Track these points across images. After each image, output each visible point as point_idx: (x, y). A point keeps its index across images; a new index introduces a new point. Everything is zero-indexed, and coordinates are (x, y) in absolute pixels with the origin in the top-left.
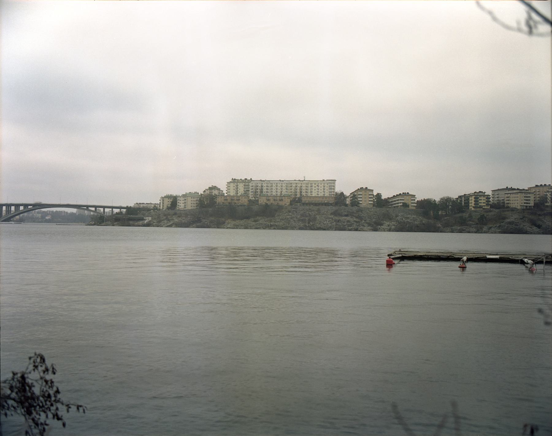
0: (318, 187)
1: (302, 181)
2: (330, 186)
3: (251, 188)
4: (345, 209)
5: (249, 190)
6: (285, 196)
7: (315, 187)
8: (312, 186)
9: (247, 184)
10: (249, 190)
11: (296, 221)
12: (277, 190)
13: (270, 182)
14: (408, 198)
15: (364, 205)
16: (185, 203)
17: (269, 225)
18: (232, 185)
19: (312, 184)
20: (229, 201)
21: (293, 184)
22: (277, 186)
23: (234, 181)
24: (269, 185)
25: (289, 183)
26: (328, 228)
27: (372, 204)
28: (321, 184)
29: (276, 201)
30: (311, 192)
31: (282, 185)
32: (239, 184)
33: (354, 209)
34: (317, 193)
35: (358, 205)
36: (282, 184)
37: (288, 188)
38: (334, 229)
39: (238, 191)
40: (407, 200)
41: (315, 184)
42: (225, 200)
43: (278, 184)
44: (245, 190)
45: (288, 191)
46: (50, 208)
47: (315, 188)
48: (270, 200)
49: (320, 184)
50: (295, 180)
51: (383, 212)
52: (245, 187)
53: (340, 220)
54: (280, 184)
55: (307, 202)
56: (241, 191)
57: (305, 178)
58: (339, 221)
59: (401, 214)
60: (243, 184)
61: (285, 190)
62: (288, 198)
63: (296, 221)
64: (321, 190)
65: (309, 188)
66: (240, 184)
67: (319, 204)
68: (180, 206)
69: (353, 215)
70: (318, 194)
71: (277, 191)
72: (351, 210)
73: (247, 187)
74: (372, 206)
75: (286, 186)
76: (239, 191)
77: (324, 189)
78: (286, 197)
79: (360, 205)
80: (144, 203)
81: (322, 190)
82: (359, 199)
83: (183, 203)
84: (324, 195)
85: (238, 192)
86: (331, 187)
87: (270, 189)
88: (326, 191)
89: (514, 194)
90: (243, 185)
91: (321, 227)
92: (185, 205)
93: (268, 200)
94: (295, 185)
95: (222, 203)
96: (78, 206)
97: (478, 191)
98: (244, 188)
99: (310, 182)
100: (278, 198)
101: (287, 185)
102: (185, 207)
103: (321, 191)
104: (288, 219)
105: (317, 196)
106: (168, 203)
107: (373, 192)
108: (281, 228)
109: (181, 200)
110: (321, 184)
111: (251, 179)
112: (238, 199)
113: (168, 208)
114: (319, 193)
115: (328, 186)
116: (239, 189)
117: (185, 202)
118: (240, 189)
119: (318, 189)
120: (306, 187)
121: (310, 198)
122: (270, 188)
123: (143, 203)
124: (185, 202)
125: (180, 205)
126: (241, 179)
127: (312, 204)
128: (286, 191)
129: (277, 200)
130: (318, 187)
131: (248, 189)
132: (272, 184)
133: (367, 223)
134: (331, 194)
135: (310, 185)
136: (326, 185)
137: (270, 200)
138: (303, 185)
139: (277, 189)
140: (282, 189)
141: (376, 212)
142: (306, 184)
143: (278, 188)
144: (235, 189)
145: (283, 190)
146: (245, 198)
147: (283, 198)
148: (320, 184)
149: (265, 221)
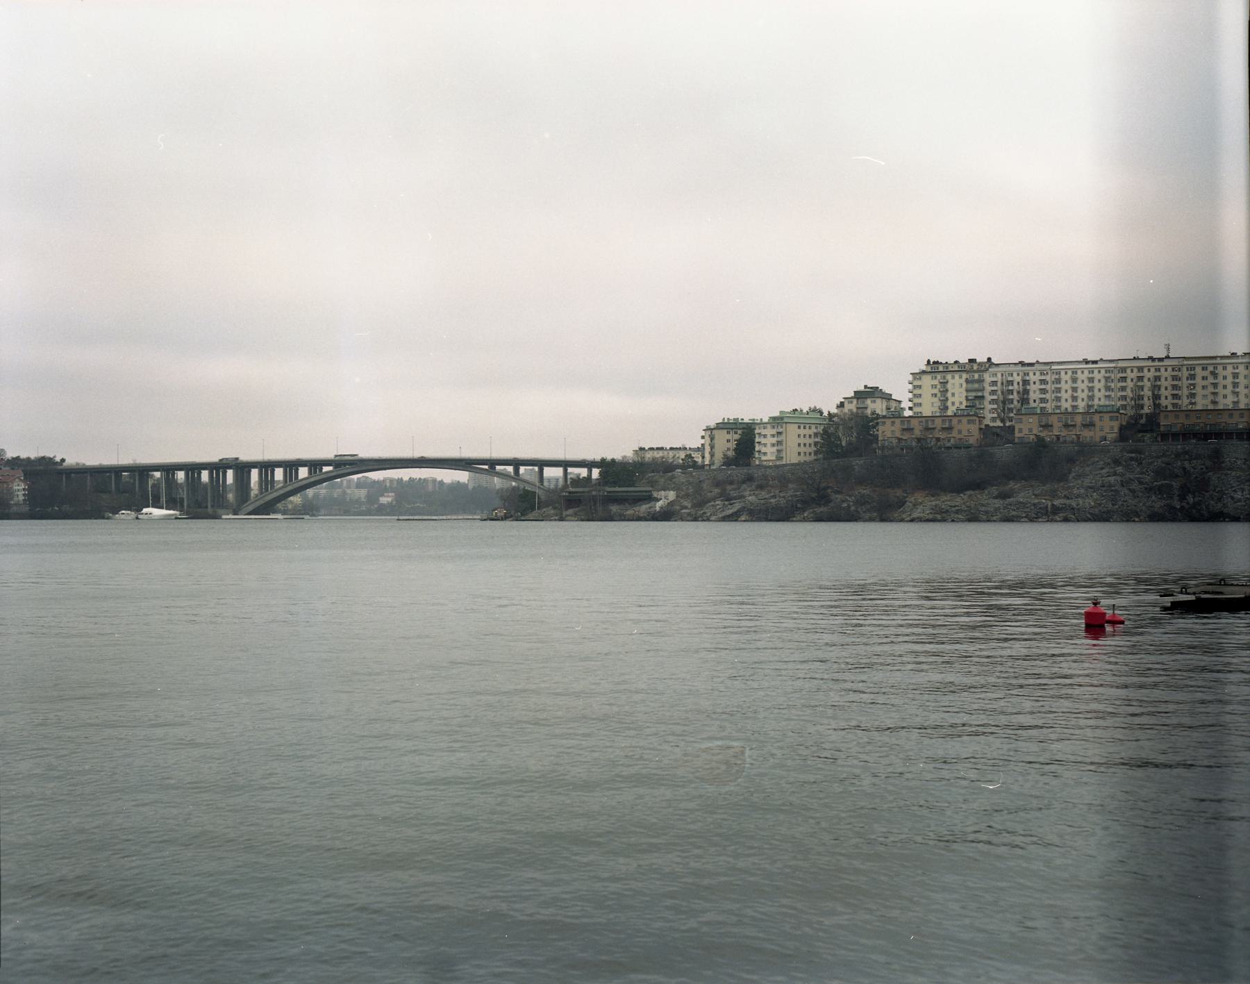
3: (989, 388)
7: (1204, 378)
8: (1192, 377)
9: (976, 376)
13: (1053, 367)
16: (779, 443)
17: (1047, 507)
18: (927, 381)
19: (1192, 368)
21: (1129, 371)
22: (1074, 380)
23: (934, 367)
24: (1048, 378)
28: (1225, 368)
30: (1193, 395)
31: (1091, 376)
32: (949, 377)
34: (1211, 397)
37: (1113, 385)
39: (947, 399)
41: (1203, 369)
42: (904, 430)
44: (970, 398)
47: (1205, 383)
48: (1094, 425)
52: (970, 386)
54: (1086, 372)
56: (957, 399)
60: (965, 376)
61: (1103, 390)
63: (1140, 494)
68: (765, 454)
70: (1214, 402)
71: (1075, 394)
73: (976, 386)
75: (1107, 379)
78: (1106, 417)
81: (1230, 388)
90: (963, 381)
91: (1225, 511)
98: (967, 391)
100: (1079, 420)
101: (1107, 375)
102: (779, 458)
104: (1110, 486)
105: (1210, 407)
113: (728, 462)
116: (949, 395)
117: (778, 442)
118: (953, 395)
122: (1053, 386)
123: (660, 446)
124: (778, 442)
126: (956, 362)
127: (1195, 435)
128: (1107, 394)
131: (980, 394)
137: (1052, 426)
138: (1096, 375)
140: (1091, 389)
142: (1173, 370)
144: (939, 395)
145: (1096, 391)
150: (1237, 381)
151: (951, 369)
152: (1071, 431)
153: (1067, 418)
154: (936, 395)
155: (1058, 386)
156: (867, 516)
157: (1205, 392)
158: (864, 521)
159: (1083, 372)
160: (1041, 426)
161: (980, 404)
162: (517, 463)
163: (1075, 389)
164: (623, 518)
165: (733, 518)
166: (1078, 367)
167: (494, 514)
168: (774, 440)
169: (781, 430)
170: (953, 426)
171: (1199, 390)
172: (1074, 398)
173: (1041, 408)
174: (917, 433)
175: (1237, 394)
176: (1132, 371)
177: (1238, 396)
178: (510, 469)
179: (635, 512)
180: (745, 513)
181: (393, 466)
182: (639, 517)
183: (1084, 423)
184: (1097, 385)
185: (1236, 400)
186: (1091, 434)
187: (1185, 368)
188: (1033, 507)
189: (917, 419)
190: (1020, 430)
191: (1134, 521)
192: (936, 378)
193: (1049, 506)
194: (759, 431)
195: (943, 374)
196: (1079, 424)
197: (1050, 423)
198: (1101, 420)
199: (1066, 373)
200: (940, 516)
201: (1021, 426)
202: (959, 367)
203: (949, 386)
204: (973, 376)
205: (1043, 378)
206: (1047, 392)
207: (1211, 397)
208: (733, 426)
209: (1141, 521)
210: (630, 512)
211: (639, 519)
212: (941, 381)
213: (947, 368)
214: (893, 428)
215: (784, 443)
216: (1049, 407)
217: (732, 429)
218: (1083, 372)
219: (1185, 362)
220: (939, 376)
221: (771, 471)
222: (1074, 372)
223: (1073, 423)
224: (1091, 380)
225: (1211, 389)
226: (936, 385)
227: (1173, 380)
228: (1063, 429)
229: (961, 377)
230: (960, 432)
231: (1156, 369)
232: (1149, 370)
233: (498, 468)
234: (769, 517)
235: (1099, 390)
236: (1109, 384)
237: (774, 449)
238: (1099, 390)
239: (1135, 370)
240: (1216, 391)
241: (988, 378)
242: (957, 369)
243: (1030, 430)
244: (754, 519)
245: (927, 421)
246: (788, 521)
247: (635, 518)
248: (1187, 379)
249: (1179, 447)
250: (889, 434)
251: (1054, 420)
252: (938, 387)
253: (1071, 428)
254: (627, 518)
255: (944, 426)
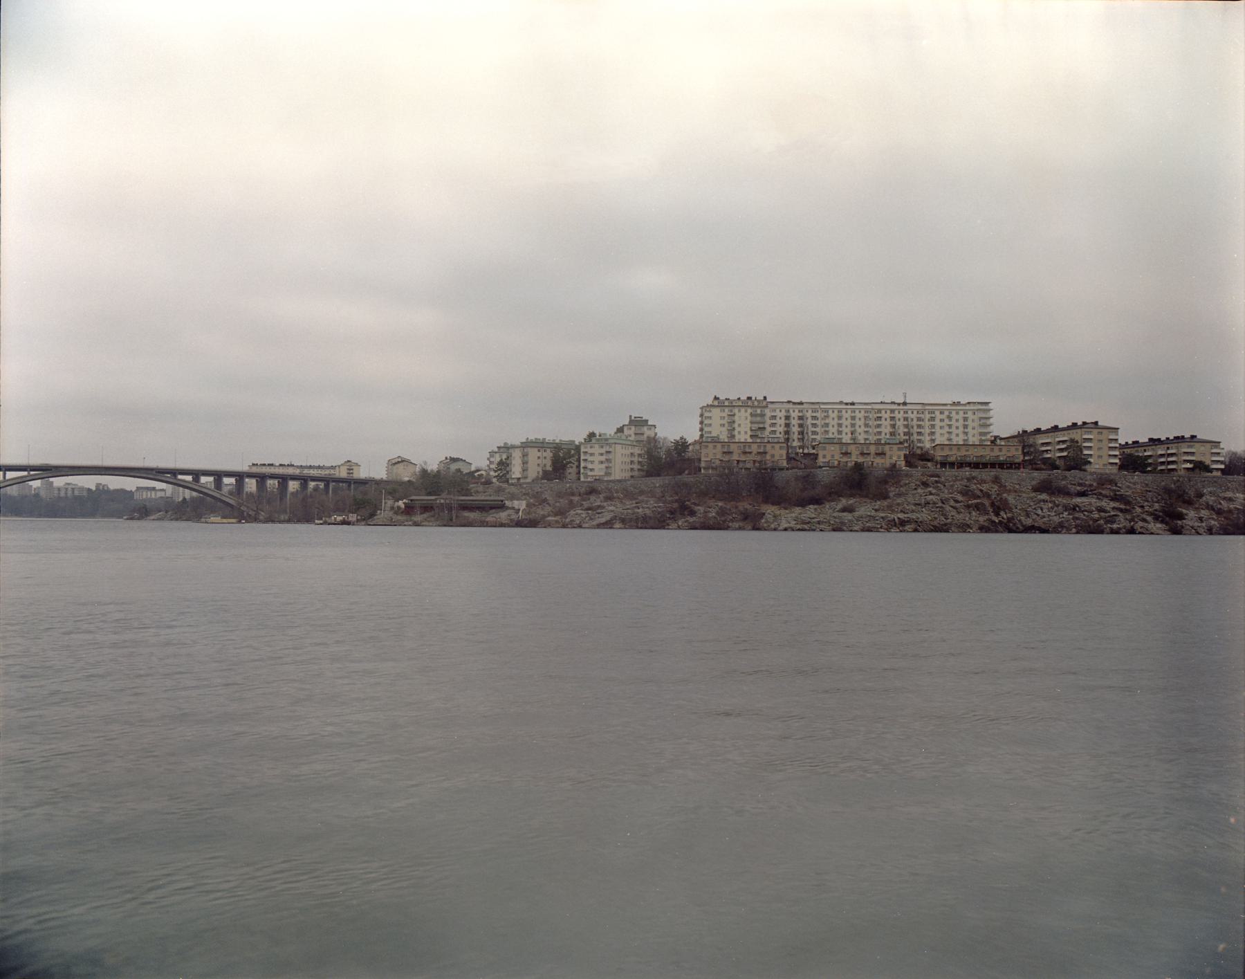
0: (950, 420)
1: (899, 404)
2: (981, 419)
3: (769, 422)
4: (1066, 477)
5: (764, 428)
6: (889, 444)
7: (942, 420)
8: (933, 419)
9: (759, 411)
10: (764, 428)
11: (963, 510)
12: (841, 427)
13: (822, 407)
14: (1203, 448)
15: (1097, 467)
16: (608, 460)
17: (894, 520)
18: (716, 413)
19: (933, 412)
20: (855, 458)
21: (883, 412)
22: (840, 418)
23: (718, 403)
24: (818, 415)
25: (874, 413)
26: (1054, 528)
27: (1116, 464)
28: (957, 413)
29: (748, 455)
30: (932, 433)
31: (853, 414)
32: (736, 410)
33: (1088, 477)
34: (947, 436)
35: (1083, 467)
36: (855, 412)
37: (870, 423)
38: (1074, 530)
39: (734, 429)
40: (1201, 454)
41: (941, 413)
42: (724, 453)
43: (844, 411)
44: (753, 428)
45: (870, 430)
46: (68, 475)
47: (942, 424)
48: (885, 454)
49: (954, 413)
50: (882, 403)
51: (1163, 483)
52: (755, 419)
53: (1078, 506)
54: (849, 411)
55: (952, 459)
56: (742, 430)
57: (905, 397)
58: (1074, 509)
59: (1209, 489)
60: (749, 410)
61: (863, 427)
62: (899, 449)
63: (963, 510)
64: (957, 428)
65: (927, 423)
66: (739, 411)
67: (983, 464)
68: (592, 470)
69: (1101, 494)
70: (950, 440)
71: (840, 429)
72: (1082, 480)
73: (758, 419)
74: (1115, 469)
75: (866, 418)
76: (737, 429)
77: (965, 427)
78: (895, 447)
79: (1087, 467)
80: (272, 465)
81: (961, 429)
82: (1086, 452)
83: (602, 462)
84: (964, 440)
85: (736, 433)
86: (983, 421)
87: (823, 426)
88: (969, 430)
89: (957, 441)
90: (748, 414)
91: (1036, 524)
92: (607, 467)
93: (846, 454)
94: (888, 415)
95: (718, 462)
96: (154, 472)
97: (1143, 439)
98: (751, 423)
99: (927, 407)
100: (873, 449)
101: (866, 415)
102: (608, 474)
103: (957, 431)
104: (934, 503)
105: (947, 443)
106: (538, 462)
107: (1117, 435)
108: (932, 528)
109: (592, 454)
110: (957, 413)
111: (765, 398)
112: (761, 450)
113: (546, 475)
114: (953, 437)
115: (975, 417)
116: (736, 425)
117: (607, 460)
118: (739, 425)
119: (950, 426)
120: (919, 419)
121: (958, 448)
122: (823, 422)
123: (271, 463)
124: (607, 460)
125: (590, 466)
126: (739, 399)
127: (969, 464)
128: (866, 429)
129: (869, 454)
130: (950, 420)
131: (761, 426)
132: (826, 411)
133: (1150, 514)
134: (983, 438)
135: (928, 416)
136: (970, 415)
137: (850, 453)
138: (857, 414)
139: (840, 425)
140: (853, 425)
141: (1147, 485)
142: (918, 412)
143: (843, 421)
144: (726, 425)
145: (857, 427)
146: (781, 448)
147: (887, 448)
148: (954, 413)
149: (876, 510)
150: (966, 423)
151: (734, 404)
152: (866, 458)
153: (863, 448)
154: (724, 425)
155: (933, 423)
156: (737, 525)
157: (942, 431)
158: (733, 530)
159: (860, 412)
160: (842, 453)
161: (761, 434)
162: (197, 474)
163: (840, 425)
164: (484, 524)
165: (608, 525)
166: (835, 407)
167: (333, 518)
168: (603, 458)
169: (611, 450)
170: (767, 451)
171: (937, 430)
172: (840, 432)
173: (839, 439)
174: (854, 458)
175: (966, 433)
176: (886, 412)
177: (967, 435)
178: (189, 478)
179: (497, 519)
180: (618, 522)
181: (97, 473)
182: (502, 523)
183: (877, 452)
184: (858, 423)
185: (966, 438)
186: (883, 461)
187: (927, 412)
188: (882, 520)
189: (735, 444)
190: (824, 456)
191: (969, 532)
192: (724, 411)
193: (896, 520)
194: (586, 450)
195: (730, 408)
196: (755, 452)
197: (849, 452)
198: (890, 450)
199: (833, 412)
200: (806, 526)
201: (825, 452)
202: (742, 403)
203: (736, 418)
204: (756, 411)
205: (814, 414)
206: (818, 426)
207: (947, 436)
208: (541, 445)
209: (974, 532)
210: (490, 519)
211: (502, 525)
212: (729, 413)
213: (732, 403)
214: (714, 451)
215: (613, 461)
216: (846, 438)
217: (542, 447)
218: (860, 412)
219: (927, 407)
220: (726, 410)
221: (613, 485)
222: (840, 411)
223: (868, 452)
224: (853, 418)
225: (947, 429)
226: (724, 417)
227: (918, 421)
228: (860, 457)
229: (746, 411)
230: (773, 456)
231: (904, 412)
232: (899, 413)
233: (180, 477)
234: (640, 525)
235: (860, 426)
236: (867, 422)
237: (603, 466)
238: (860, 426)
239: (888, 412)
240: (950, 430)
241: (768, 413)
242: (741, 404)
243: (833, 456)
244: (627, 527)
245: (744, 446)
246: (664, 529)
247: (498, 525)
248: (929, 420)
249: (967, 473)
250: (711, 456)
251: (852, 449)
252: (726, 418)
253: (866, 456)
254: (490, 525)
255: (759, 451)
